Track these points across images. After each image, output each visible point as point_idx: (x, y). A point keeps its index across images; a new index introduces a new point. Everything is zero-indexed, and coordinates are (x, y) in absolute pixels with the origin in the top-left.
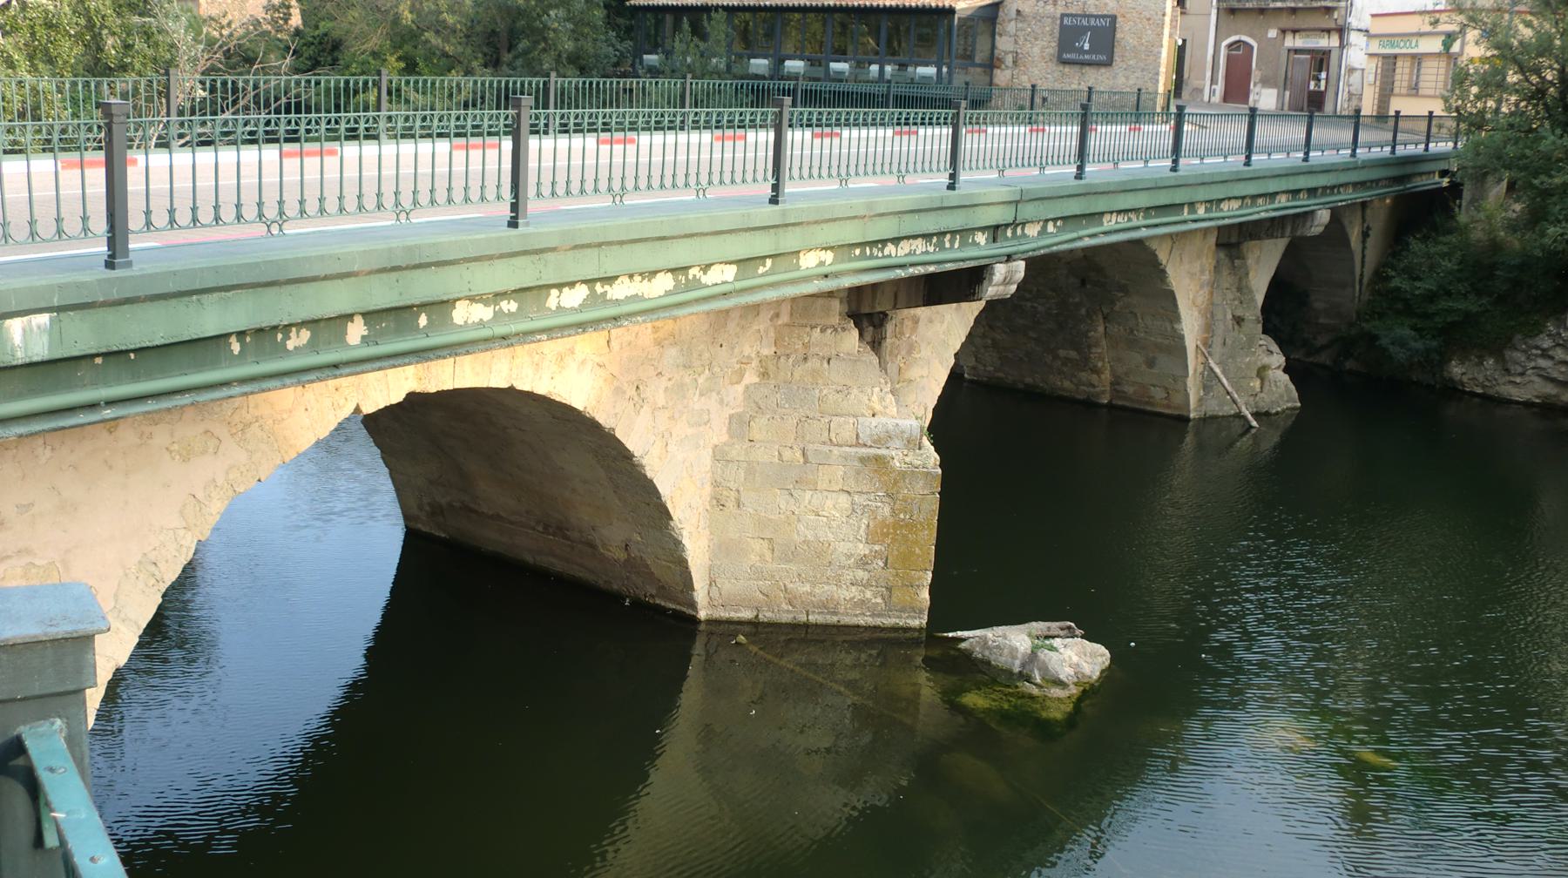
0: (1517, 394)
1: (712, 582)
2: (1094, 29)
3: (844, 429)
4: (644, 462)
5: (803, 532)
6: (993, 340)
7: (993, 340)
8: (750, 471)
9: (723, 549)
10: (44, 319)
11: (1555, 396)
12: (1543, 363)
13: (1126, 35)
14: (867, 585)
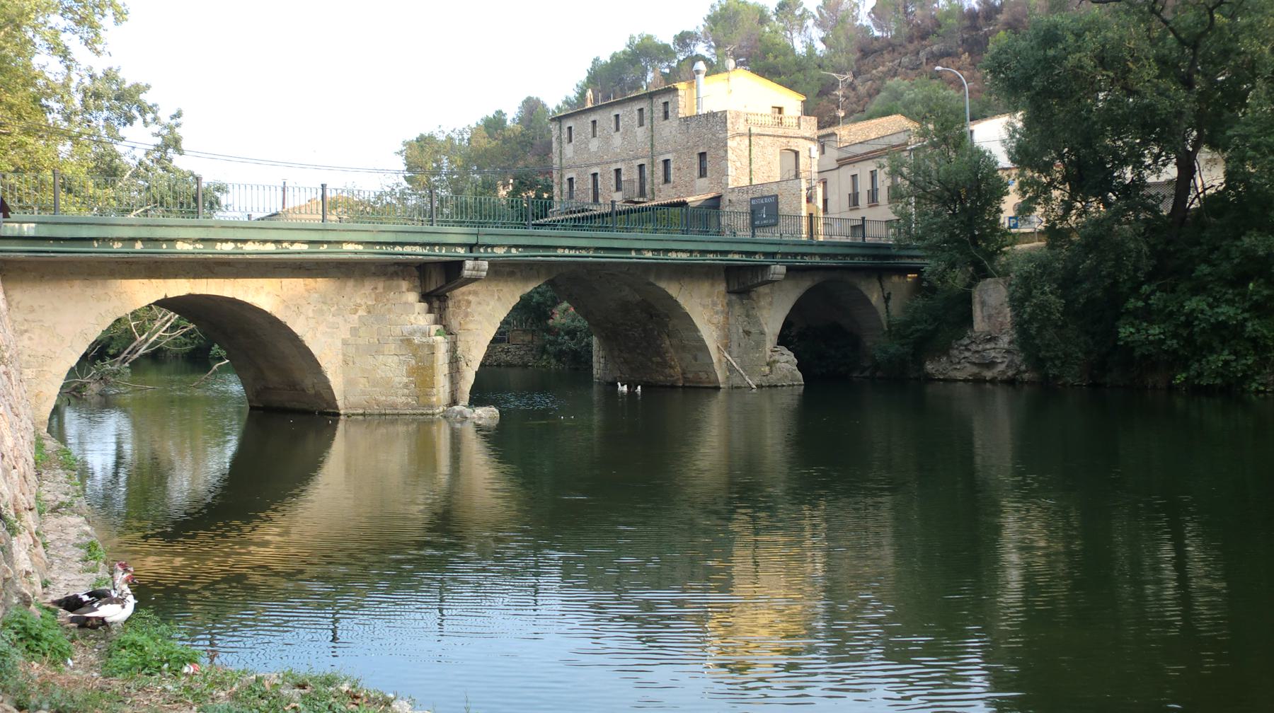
0: (960, 375)
1: (345, 398)
2: (767, 205)
3: (397, 330)
4: (304, 339)
5: (380, 374)
6: (624, 358)
7: (624, 358)
8: (357, 349)
9: (349, 383)
10: (33, 225)
11: (978, 373)
12: (967, 354)
13: (784, 208)
14: (408, 396)
